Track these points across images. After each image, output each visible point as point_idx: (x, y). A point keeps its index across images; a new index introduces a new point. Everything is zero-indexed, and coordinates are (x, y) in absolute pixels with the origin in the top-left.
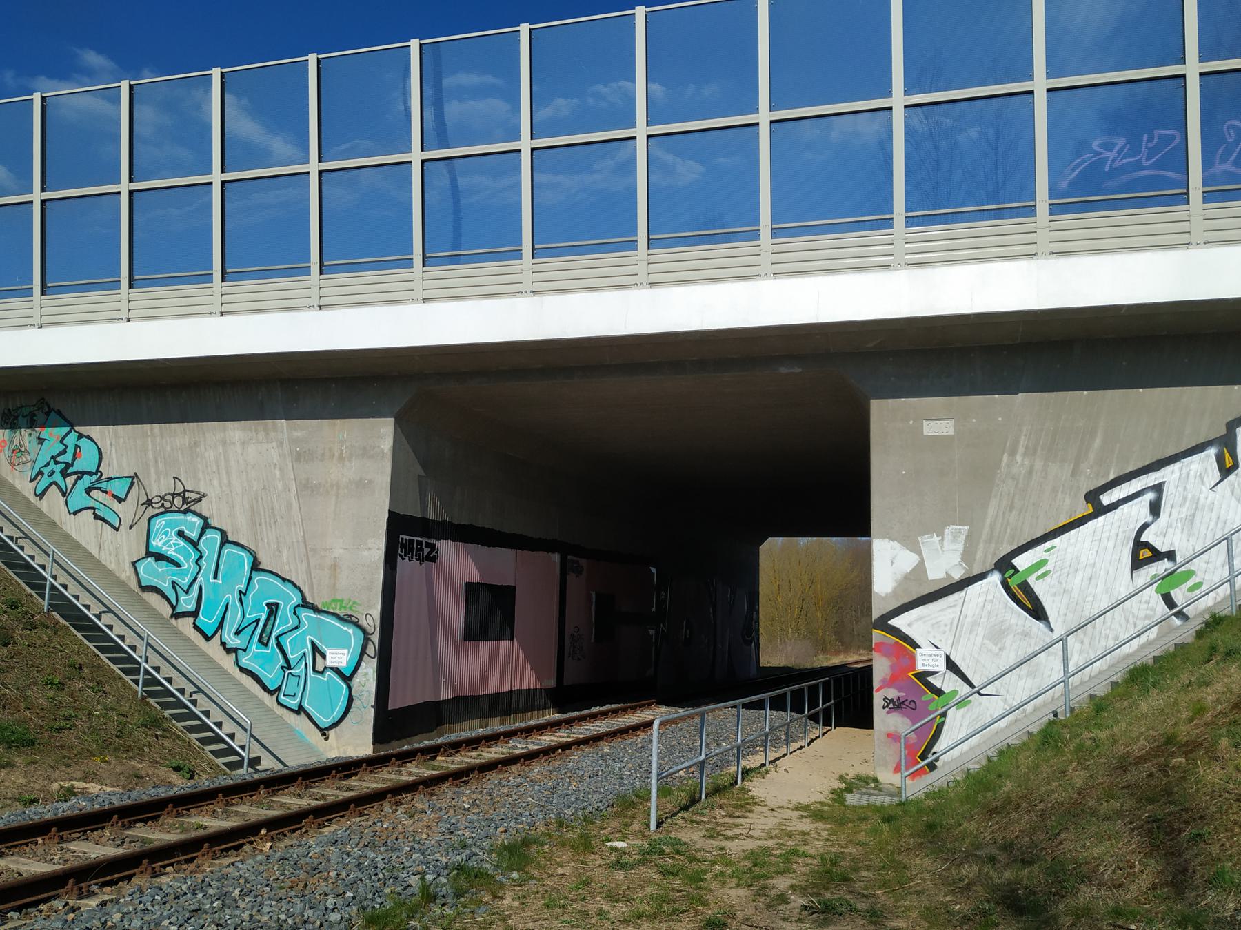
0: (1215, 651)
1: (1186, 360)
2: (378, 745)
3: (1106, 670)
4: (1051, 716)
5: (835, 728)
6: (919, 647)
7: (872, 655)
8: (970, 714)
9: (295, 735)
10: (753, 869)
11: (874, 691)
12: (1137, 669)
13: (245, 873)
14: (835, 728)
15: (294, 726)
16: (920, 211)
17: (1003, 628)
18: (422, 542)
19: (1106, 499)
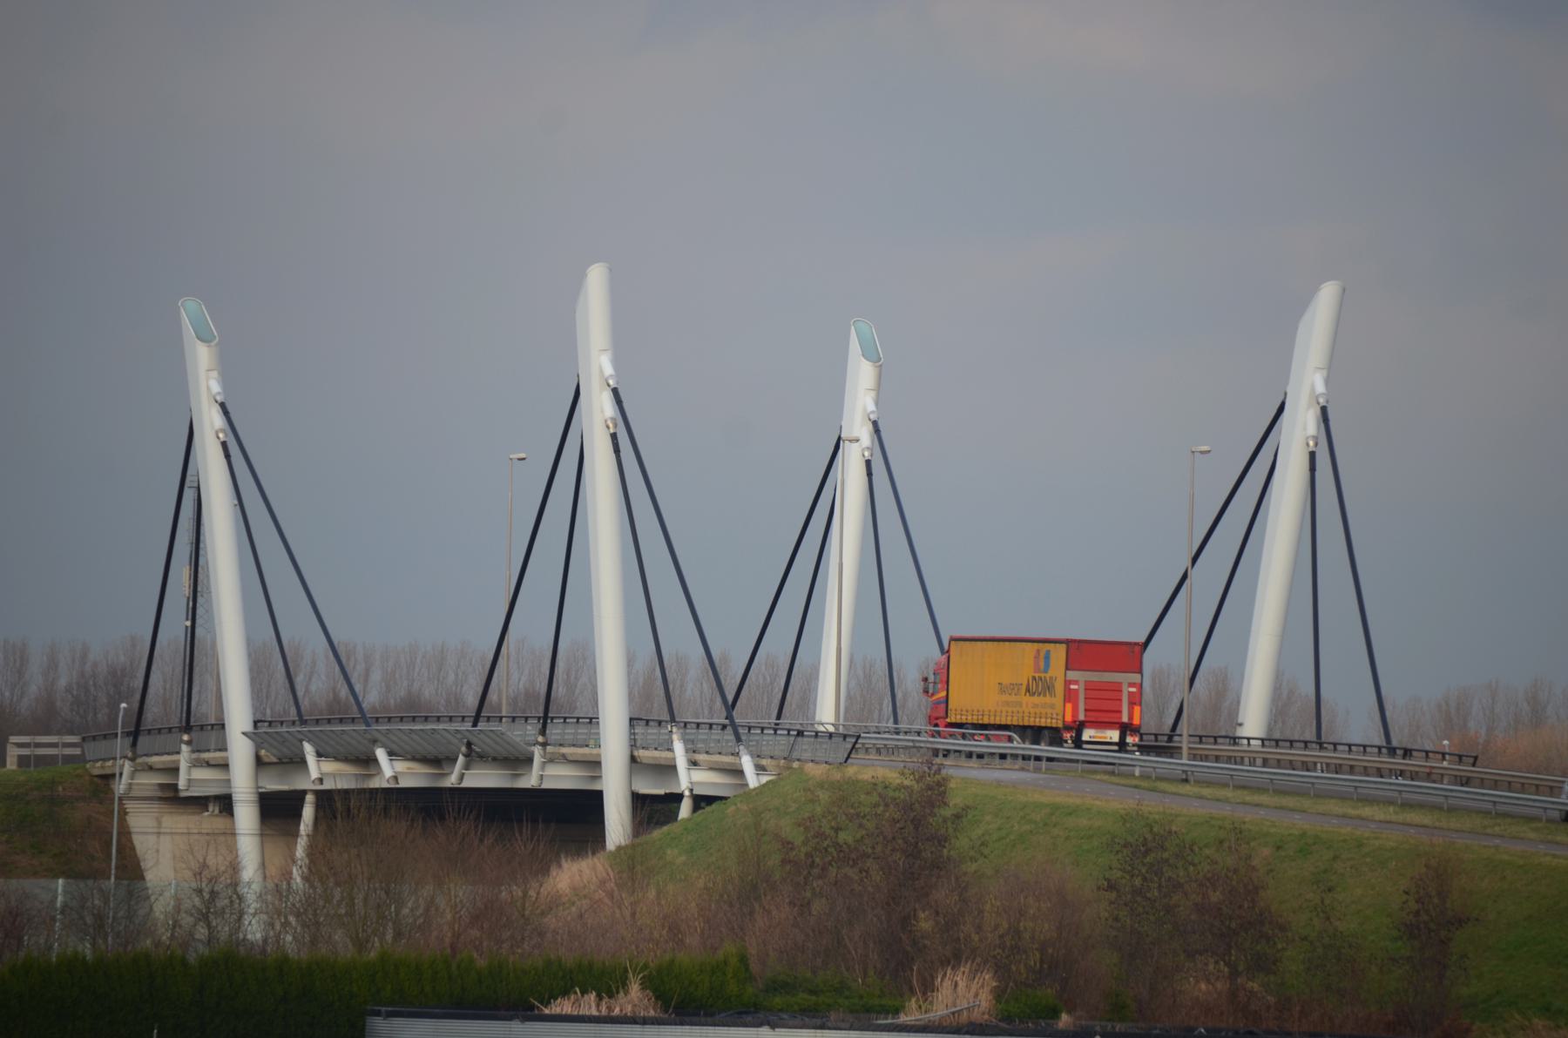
0: (813, 816)
1: (1050, 951)
2: (673, 764)
3: (210, 933)
4: (1240, 721)
5: (583, 996)
6: (243, 733)
7: (737, 754)
8: (637, 882)
9: (618, 993)
10: (299, 862)
11: (397, 786)
12: (643, 989)
13: (837, 830)
14: (583, 996)
15: (804, 1018)
16: (116, 863)
17: (413, 898)
18: (1053, 694)
19: (588, 720)
